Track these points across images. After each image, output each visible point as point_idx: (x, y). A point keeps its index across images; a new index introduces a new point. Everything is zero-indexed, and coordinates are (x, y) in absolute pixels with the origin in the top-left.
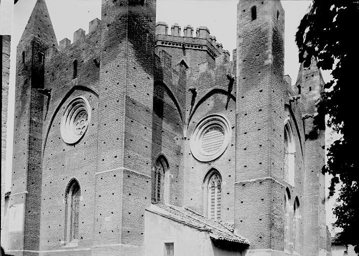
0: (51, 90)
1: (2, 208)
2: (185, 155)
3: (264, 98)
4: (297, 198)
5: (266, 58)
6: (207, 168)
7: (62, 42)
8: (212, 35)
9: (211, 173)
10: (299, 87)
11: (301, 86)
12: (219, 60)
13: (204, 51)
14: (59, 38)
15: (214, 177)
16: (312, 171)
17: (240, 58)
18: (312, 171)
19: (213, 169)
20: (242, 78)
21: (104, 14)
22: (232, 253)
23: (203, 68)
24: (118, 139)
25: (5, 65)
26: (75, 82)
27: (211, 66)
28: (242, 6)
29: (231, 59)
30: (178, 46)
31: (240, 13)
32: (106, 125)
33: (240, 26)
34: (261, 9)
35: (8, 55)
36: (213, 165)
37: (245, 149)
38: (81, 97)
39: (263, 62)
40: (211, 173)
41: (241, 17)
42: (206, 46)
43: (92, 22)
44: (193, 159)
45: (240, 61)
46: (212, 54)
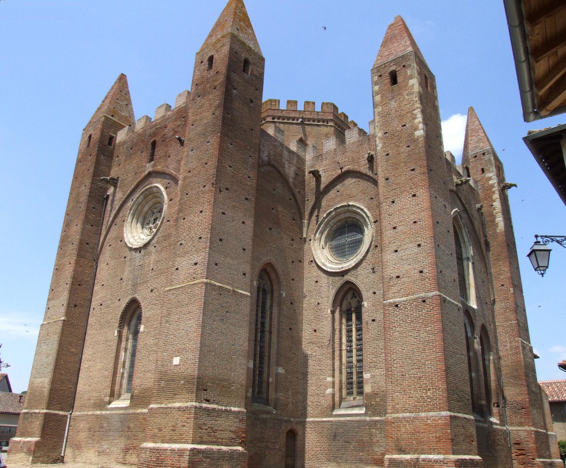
0: (118, 178)
2: (306, 263)
4: (483, 327)
5: (416, 129)
6: (339, 281)
10: (467, 169)
11: (470, 167)
12: (351, 136)
13: (330, 126)
16: (503, 285)
18: (503, 285)
19: (348, 282)
22: (425, 63)
24: (200, 238)
26: (149, 168)
30: (295, 122)
32: (186, 220)
35: (268, 274)
36: (347, 277)
37: (396, 251)
39: (413, 134)
44: (316, 268)
46: (340, 134)
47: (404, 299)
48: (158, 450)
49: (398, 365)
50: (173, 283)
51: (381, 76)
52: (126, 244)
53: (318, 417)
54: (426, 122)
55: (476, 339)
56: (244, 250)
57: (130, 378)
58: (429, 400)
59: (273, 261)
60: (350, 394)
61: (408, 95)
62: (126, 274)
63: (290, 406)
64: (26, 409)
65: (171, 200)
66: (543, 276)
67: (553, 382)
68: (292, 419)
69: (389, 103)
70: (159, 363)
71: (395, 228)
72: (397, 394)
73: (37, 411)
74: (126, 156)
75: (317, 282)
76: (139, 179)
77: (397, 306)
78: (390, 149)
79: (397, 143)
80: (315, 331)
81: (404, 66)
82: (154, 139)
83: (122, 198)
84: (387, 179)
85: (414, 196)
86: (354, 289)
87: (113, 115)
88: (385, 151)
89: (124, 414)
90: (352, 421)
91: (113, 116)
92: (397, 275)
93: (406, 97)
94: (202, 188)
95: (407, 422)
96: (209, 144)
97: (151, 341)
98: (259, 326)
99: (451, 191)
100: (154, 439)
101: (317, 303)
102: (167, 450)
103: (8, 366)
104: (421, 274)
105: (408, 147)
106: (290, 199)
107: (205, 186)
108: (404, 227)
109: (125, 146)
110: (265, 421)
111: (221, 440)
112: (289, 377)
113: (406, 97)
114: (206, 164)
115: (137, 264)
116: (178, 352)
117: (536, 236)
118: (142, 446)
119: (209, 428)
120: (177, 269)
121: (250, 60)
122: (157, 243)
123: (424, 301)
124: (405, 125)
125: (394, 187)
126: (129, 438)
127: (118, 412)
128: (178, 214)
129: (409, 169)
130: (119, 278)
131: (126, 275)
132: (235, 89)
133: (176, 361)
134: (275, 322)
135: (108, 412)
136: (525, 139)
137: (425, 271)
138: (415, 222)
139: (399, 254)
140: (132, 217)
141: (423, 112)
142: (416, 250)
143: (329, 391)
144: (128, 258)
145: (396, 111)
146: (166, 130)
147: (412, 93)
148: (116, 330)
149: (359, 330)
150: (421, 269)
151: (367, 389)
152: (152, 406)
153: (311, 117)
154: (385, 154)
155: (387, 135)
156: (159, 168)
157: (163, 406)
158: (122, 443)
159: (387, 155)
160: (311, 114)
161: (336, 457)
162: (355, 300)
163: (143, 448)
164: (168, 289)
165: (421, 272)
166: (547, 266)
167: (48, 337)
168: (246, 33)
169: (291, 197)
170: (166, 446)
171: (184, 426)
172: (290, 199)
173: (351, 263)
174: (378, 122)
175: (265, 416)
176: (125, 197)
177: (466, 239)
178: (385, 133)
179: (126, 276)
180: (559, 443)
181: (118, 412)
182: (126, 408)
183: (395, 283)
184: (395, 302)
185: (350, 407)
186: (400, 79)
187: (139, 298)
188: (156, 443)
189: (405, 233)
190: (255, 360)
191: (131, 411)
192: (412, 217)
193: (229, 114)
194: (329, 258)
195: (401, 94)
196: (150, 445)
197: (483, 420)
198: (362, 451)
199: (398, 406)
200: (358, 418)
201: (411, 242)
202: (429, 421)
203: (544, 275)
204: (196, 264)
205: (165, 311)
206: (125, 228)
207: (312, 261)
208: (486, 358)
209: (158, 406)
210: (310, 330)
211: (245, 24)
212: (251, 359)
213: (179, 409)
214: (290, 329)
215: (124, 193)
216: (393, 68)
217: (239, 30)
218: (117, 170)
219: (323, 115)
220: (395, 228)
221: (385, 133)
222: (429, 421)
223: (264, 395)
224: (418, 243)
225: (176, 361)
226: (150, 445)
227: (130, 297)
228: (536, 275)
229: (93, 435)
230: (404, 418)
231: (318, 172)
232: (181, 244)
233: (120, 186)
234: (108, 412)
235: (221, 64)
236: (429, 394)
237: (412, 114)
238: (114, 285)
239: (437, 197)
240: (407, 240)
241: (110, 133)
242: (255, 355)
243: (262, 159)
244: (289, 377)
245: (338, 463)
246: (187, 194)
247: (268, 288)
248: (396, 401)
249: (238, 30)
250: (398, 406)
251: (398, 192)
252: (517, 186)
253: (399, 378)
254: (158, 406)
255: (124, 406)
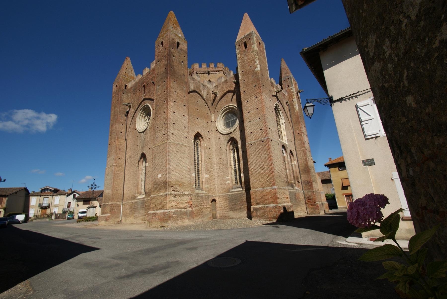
6: (228, 137)
24: (165, 123)
36: (232, 135)
37: (250, 122)
39: (255, 70)
47: (255, 141)
48: (155, 214)
49: (254, 169)
50: (156, 144)
51: (239, 45)
52: (137, 131)
53: (224, 193)
55: (384, 263)
56: (185, 127)
58: (267, 182)
61: (252, 52)
62: (139, 143)
63: (212, 190)
64: (104, 203)
65: (153, 110)
66: (311, 119)
68: (213, 195)
69: (243, 57)
70: (153, 178)
71: (249, 112)
72: (254, 181)
73: (107, 203)
74: (133, 93)
75: (219, 139)
76: (140, 102)
77: (252, 145)
78: (245, 78)
79: (248, 75)
80: (220, 159)
81: (250, 39)
82: (143, 84)
83: (134, 112)
84: (245, 92)
85: (256, 97)
86: (234, 140)
87: (125, 75)
88: (243, 80)
89: (143, 200)
90: (238, 194)
91: (125, 76)
92: (251, 132)
93: (251, 53)
94: (164, 102)
95: (259, 192)
96: (165, 82)
97: (151, 169)
98: (196, 159)
99: (273, 96)
100: (153, 209)
101: (220, 147)
102: (158, 213)
103: (99, 187)
104: (261, 130)
105: (253, 76)
106: (205, 105)
107: (165, 101)
108: (252, 111)
109: (132, 89)
110: (202, 197)
111: (181, 207)
112: (211, 178)
113: (251, 53)
114: (164, 91)
115: (143, 138)
116: (160, 173)
117: (307, 100)
118: (149, 213)
119: (175, 202)
120: (157, 138)
121: (180, 43)
122: (150, 129)
123: (263, 142)
124: (251, 67)
125: (248, 94)
126: (146, 210)
127: (141, 200)
128: (155, 115)
129: (254, 86)
130: (136, 145)
131: (139, 144)
132: (174, 56)
133: (160, 176)
135: (137, 200)
136: (301, 53)
137: (263, 129)
138: (257, 109)
139: (251, 123)
142: (258, 120)
144: (139, 136)
145: (247, 61)
146: (148, 80)
147: (254, 51)
148: (137, 167)
150: (261, 128)
152: (151, 196)
153: (213, 70)
154: (243, 80)
155: (243, 72)
156: (147, 97)
157: (156, 195)
158: (143, 212)
159: (244, 81)
160: (212, 69)
161: (232, 209)
162: (236, 144)
163: (149, 214)
164: (154, 147)
165: (261, 129)
167: (109, 173)
168: (177, 30)
169: (206, 104)
170: (158, 211)
171: (164, 202)
172: (205, 105)
173: (232, 130)
174: (240, 67)
175: (201, 195)
176: (135, 111)
177: (281, 115)
178: (243, 71)
179: (139, 144)
180: (245, 48)
181: (141, 200)
182: (144, 198)
183: (250, 135)
184: (251, 143)
185: (237, 188)
186: (248, 46)
187: (145, 152)
188: (154, 211)
189: (253, 114)
190: (195, 173)
191: (146, 199)
192: (256, 107)
193: (172, 68)
194: (224, 129)
195: (248, 52)
196: (153, 212)
197: (293, 189)
198: (243, 205)
199: (255, 186)
200: (240, 192)
201: (256, 117)
202: (268, 191)
203: (311, 118)
204: (164, 135)
205: (153, 156)
206: (136, 124)
207: (217, 130)
208: (293, 164)
209: (154, 195)
210: (218, 159)
211: (176, 26)
212: (193, 172)
213: (162, 196)
214: (210, 159)
215: (134, 109)
216: (245, 41)
217: (174, 28)
218: (130, 100)
219: (218, 69)
220: (249, 112)
221: (243, 71)
222: (268, 191)
224: (259, 117)
225: (160, 176)
226: (153, 212)
227: (141, 152)
229: (132, 210)
230: (258, 190)
231: (216, 93)
232: (158, 127)
233: (132, 107)
234: (137, 200)
236: (267, 180)
237: (254, 61)
238: (135, 148)
239: (267, 97)
240: (254, 117)
241: (125, 84)
243: (191, 89)
244: (211, 178)
245: (234, 211)
246: (158, 106)
248: (254, 184)
249: (173, 28)
250: (255, 186)
251: (249, 96)
252: (316, 162)
253: (254, 174)
254: (154, 195)
255: (143, 197)
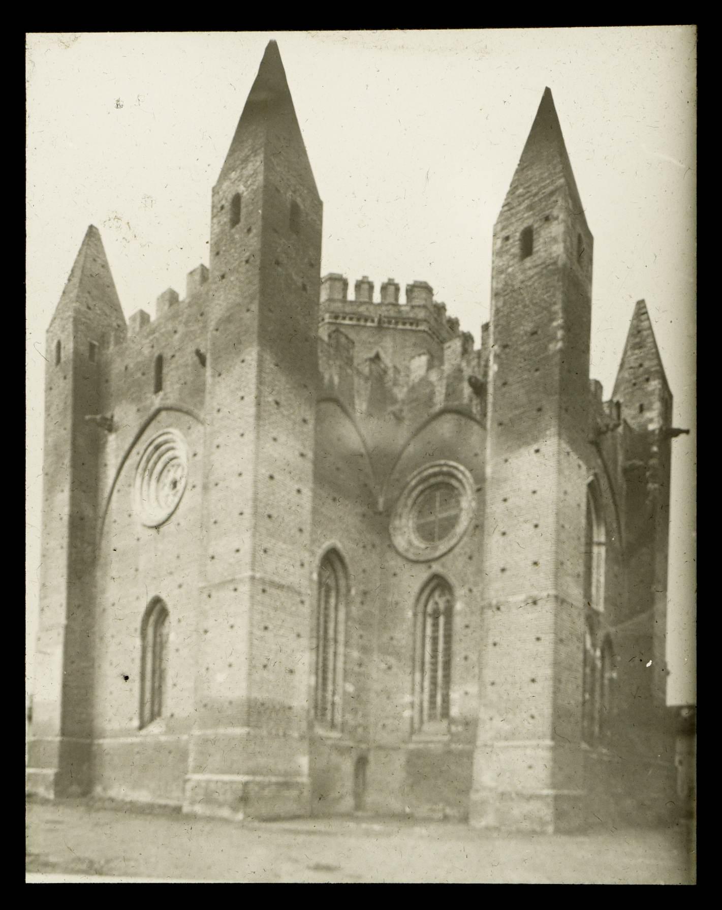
1: (695, 784)
3: (559, 160)
6: (423, 575)
7: (133, 319)
8: (438, 298)
9: (432, 585)
14: (129, 311)
15: (437, 594)
17: (496, 341)
20: (499, 383)
21: (217, 254)
23: (419, 364)
25: (693, 880)
27: (435, 360)
28: (503, 229)
29: (477, 346)
31: (499, 242)
33: (497, 272)
34: (543, 233)
36: (436, 568)
38: (166, 430)
39: (546, 348)
40: (432, 585)
41: (498, 253)
42: (425, 320)
43: (191, 273)
45: (496, 347)
54: (567, 327)
57: (446, 669)
59: (339, 546)
60: (432, 717)
67: (450, 827)
134: (341, 628)
140: (141, 477)
141: (565, 310)
143: (407, 713)
149: (448, 637)
151: (454, 711)
166: (341, 283)
173: (443, 547)
223: (329, 717)
228: (177, 289)
235: (254, 214)
237: (549, 311)
242: (317, 669)
247: (331, 582)
